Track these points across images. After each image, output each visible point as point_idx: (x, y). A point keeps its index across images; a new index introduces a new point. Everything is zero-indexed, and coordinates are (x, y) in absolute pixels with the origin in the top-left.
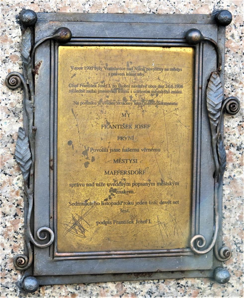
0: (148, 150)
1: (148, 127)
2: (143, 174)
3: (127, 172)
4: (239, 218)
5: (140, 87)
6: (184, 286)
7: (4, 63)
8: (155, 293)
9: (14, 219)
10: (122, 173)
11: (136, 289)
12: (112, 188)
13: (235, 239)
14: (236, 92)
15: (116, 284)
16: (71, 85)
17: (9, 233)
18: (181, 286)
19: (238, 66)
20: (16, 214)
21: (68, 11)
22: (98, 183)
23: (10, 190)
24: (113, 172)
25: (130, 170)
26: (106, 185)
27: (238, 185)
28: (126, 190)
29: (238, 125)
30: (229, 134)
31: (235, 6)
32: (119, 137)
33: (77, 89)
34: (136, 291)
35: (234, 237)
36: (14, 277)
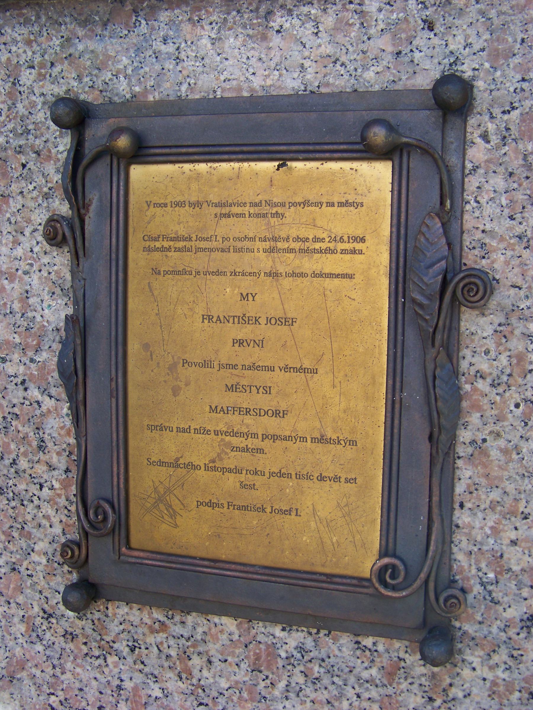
0: (292, 370)
1: (292, 322)
2: (283, 417)
3: (252, 411)
4: (492, 531)
5: (275, 239)
6: (370, 650)
7: (47, 199)
8: (311, 651)
9: (64, 476)
10: (241, 413)
11: (274, 637)
12: (222, 440)
13: (480, 574)
14: (492, 259)
15: (238, 621)
16: (146, 238)
17: (59, 500)
18: (364, 648)
19: (498, 202)
20: (67, 469)
21: (151, 98)
22: (198, 427)
23: (57, 426)
24: (225, 409)
25: (258, 407)
26: (213, 433)
27: (492, 461)
28: (249, 446)
29: (496, 331)
30: (475, 350)
31: (491, 70)
32: (235, 341)
33: (158, 244)
34: (275, 641)
35: (479, 570)
36: (68, 576)
